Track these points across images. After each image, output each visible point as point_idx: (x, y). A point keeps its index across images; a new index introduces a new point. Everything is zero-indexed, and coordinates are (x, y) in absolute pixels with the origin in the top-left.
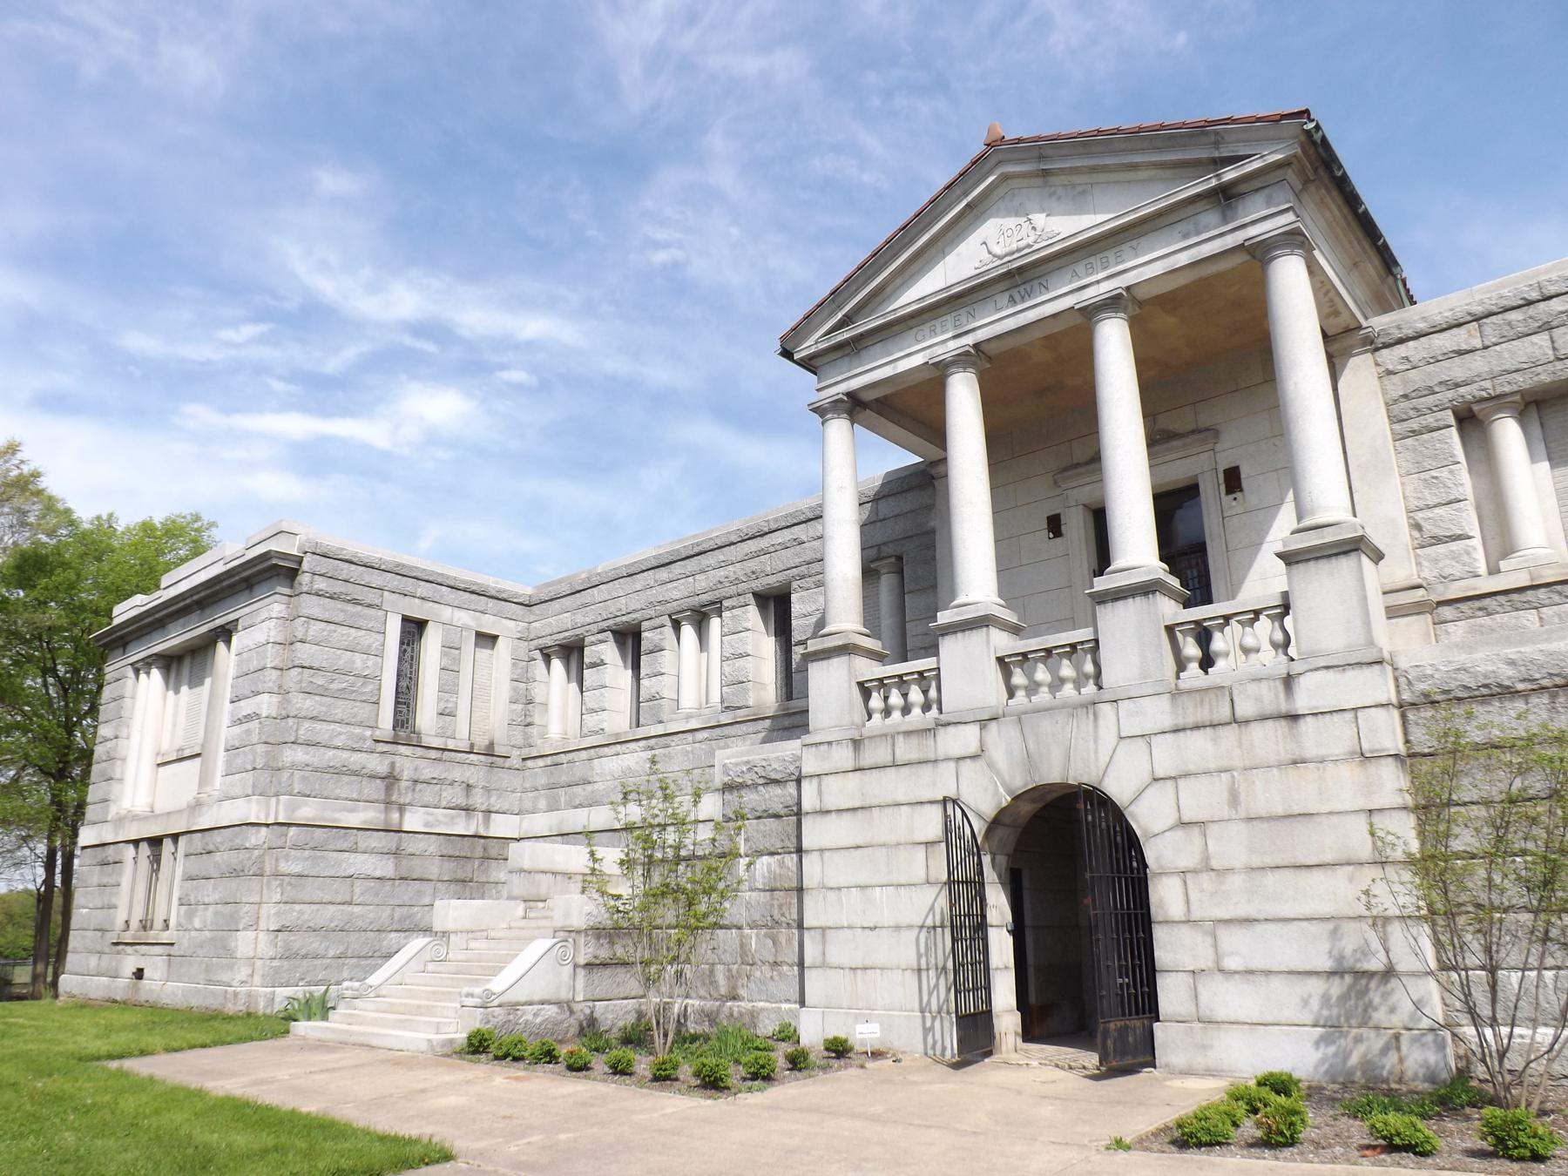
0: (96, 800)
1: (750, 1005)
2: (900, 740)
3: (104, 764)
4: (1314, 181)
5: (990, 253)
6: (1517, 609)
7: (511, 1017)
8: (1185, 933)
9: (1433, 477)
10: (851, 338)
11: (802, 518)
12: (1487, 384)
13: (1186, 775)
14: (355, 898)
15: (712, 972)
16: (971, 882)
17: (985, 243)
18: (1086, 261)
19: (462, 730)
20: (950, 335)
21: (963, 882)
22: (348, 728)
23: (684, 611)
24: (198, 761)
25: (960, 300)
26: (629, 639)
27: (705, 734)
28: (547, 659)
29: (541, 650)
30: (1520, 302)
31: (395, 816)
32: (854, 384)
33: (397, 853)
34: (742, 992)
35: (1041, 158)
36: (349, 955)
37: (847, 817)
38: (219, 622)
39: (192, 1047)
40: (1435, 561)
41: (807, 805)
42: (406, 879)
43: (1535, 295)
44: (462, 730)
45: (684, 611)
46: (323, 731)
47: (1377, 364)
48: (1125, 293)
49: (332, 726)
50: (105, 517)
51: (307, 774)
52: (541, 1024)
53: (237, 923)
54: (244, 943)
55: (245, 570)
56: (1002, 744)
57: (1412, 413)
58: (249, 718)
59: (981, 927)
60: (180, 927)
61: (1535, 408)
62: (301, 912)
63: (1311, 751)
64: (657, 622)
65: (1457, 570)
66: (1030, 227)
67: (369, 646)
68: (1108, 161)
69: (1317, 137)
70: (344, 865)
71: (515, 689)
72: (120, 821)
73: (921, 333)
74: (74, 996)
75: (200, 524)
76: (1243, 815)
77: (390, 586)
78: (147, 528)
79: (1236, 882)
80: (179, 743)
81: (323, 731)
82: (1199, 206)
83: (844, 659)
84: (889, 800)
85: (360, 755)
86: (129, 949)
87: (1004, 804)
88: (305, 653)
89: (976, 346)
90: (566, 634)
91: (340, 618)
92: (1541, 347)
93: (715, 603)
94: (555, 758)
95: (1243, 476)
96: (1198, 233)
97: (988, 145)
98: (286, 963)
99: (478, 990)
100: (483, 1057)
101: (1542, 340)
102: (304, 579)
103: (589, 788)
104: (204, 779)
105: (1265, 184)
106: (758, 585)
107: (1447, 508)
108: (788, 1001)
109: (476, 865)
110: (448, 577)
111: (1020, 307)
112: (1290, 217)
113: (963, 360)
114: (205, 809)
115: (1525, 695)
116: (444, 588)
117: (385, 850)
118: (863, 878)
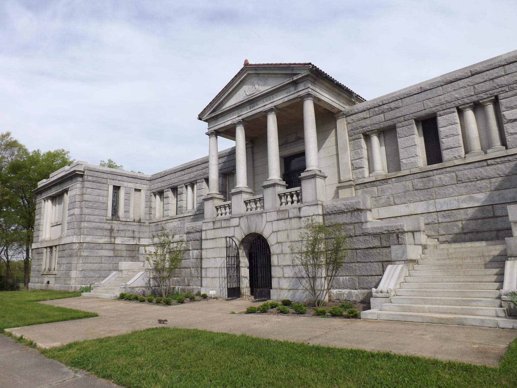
0: (36, 236)
1: (192, 287)
2: (223, 221)
3: (37, 226)
6: (373, 187)
7: (132, 290)
8: (277, 268)
12: (370, 127)
13: (279, 231)
14: (103, 261)
15: (184, 279)
20: (236, 116)
21: (233, 257)
22: (99, 217)
24: (61, 225)
26: (174, 189)
28: (155, 195)
29: (153, 193)
30: (378, 105)
31: (113, 240)
32: (216, 128)
33: (114, 250)
34: (191, 284)
36: (101, 276)
37: (211, 240)
38: (64, 188)
39: (56, 299)
40: (356, 174)
41: (203, 238)
43: (381, 104)
46: (92, 218)
47: (346, 121)
49: (94, 216)
50: (37, 151)
52: (140, 292)
53: (71, 268)
54: (74, 274)
55: (70, 175)
56: (244, 222)
57: (353, 134)
58: (72, 215)
59: (238, 267)
60: (58, 270)
61: (383, 133)
64: (181, 186)
65: (360, 176)
67: (104, 194)
68: (270, 72)
71: (146, 204)
72: (42, 242)
73: (230, 115)
74: (32, 289)
75: (64, 152)
76: (289, 241)
77: (109, 178)
78: (49, 154)
80: (57, 221)
81: (92, 218)
83: (212, 200)
84: (220, 236)
85: (102, 224)
86: (45, 276)
87: (243, 238)
88: (86, 197)
89: (242, 119)
90: (159, 189)
91: (95, 187)
92: (381, 118)
93: (195, 181)
94: (157, 223)
99: (124, 284)
100: (123, 299)
101: (382, 116)
102: (85, 177)
104: (62, 230)
107: (359, 160)
109: (136, 252)
110: (126, 174)
111: (252, 109)
113: (239, 123)
114: (62, 239)
115: (346, 213)
117: (110, 249)
118: (214, 256)
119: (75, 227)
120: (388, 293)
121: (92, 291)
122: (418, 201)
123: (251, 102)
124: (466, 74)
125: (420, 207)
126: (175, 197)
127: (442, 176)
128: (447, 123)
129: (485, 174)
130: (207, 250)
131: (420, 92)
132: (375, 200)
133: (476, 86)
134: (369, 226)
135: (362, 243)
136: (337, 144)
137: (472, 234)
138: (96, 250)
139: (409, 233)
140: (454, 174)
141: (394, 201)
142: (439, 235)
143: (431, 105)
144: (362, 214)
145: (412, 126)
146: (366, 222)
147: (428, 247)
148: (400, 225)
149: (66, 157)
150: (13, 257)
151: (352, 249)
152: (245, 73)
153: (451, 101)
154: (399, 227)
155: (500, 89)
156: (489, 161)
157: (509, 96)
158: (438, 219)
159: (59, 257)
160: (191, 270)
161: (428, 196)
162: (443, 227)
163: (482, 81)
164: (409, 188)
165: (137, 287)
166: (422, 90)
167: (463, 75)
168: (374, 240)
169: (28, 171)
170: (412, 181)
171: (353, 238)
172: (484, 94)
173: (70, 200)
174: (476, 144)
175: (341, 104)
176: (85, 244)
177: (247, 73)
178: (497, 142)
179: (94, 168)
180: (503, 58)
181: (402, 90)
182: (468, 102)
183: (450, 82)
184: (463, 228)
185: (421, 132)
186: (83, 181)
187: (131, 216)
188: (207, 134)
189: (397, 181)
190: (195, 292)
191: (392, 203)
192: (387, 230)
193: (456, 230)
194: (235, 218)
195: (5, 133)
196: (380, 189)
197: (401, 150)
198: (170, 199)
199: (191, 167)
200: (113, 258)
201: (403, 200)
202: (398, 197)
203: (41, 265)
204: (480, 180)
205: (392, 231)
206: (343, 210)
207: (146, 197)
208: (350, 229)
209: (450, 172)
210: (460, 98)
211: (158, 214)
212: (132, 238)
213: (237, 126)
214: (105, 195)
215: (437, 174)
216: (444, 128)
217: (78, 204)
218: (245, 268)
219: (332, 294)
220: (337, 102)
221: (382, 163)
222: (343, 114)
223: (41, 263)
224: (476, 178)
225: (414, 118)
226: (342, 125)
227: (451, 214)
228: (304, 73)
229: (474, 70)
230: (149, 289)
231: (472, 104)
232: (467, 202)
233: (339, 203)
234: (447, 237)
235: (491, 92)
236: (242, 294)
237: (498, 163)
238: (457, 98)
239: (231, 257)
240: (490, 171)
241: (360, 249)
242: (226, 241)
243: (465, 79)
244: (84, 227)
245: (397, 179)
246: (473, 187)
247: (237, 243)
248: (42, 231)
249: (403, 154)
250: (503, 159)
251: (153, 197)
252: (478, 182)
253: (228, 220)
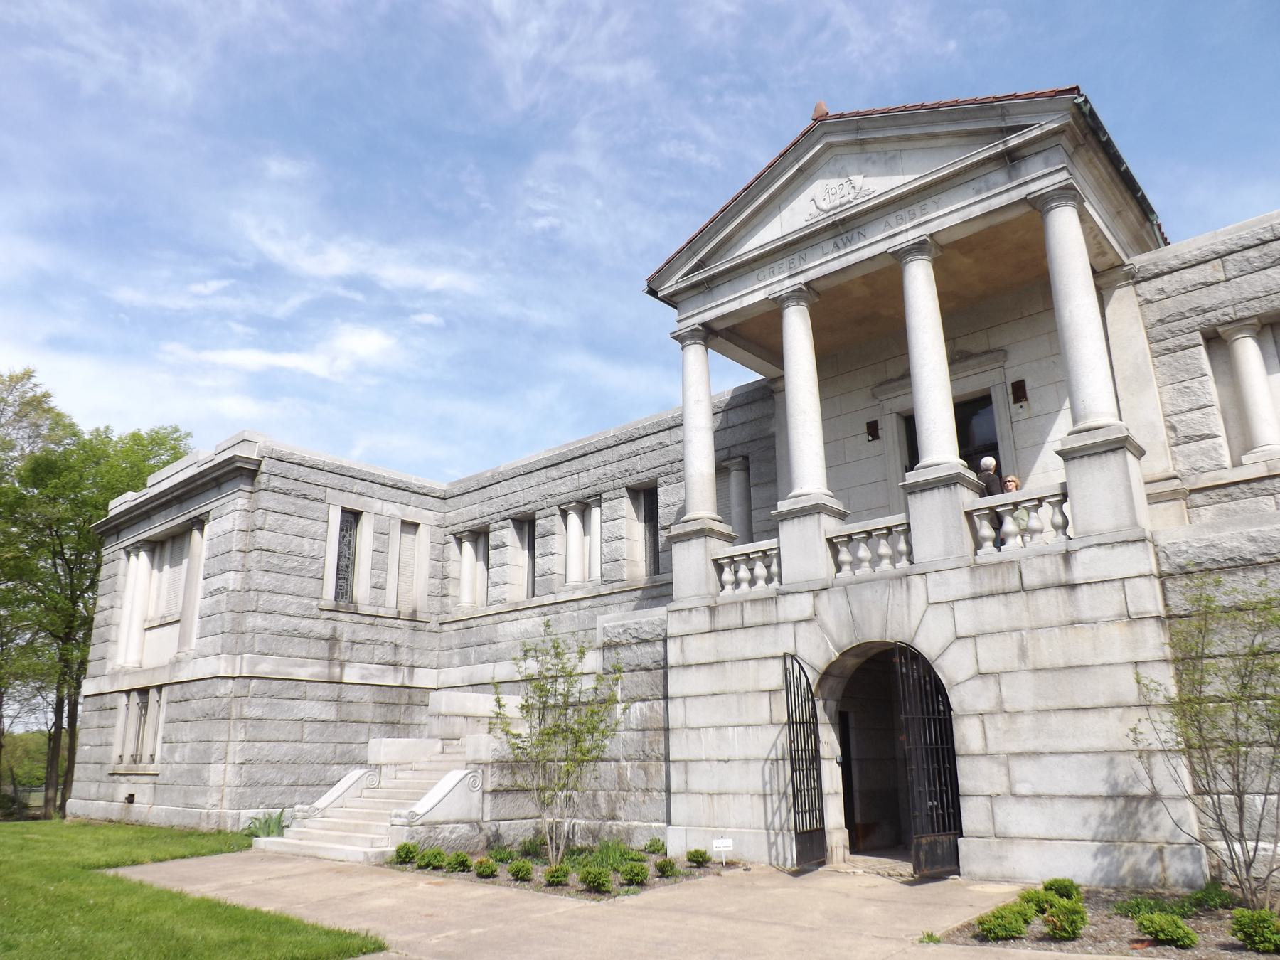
0: (96, 658)
1: (627, 823)
2: (748, 606)
3: (102, 629)
4: (1084, 144)
5: (818, 208)
6: (1257, 496)
8: (983, 764)
10: (704, 279)
11: (666, 426)
12: (1230, 310)
13: (983, 634)
14: (304, 737)
15: (595, 797)
17: (813, 200)
18: (896, 214)
19: (391, 600)
20: (786, 275)
21: (800, 723)
22: (299, 599)
24: (177, 626)
25: (793, 247)
26: (526, 525)
27: (588, 603)
28: (459, 542)
29: (454, 535)
30: (1256, 242)
31: (337, 670)
33: (338, 701)
34: (620, 813)
35: (859, 130)
36: (300, 783)
37: (705, 670)
38: (194, 514)
39: (174, 858)
40: (1188, 456)
41: (672, 660)
43: (1269, 236)
44: (391, 600)
46: (278, 601)
47: (1138, 295)
48: (928, 239)
49: (286, 598)
50: (102, 429)
51: (265, 636)
52: (456, 840)
54: (216, 773)
57: (1167, 335)
60: (163, 761)
63: (1086, 613)
64: (548, 511)
66: (851, 186)
67: (315, 533)
68: (914, 131)
69: (1086, 109)
71: (433, 567)
72: (115, 675)
74: (78, 817)
75: (178, 434)
76: (1030, 667)
77: (331, 484)
79: (1026, 722)
81: (278, 601)
82: (990, 167)
83: (702, 540)
84: (739, 656)
86: (123, 779)
87: (834, 659)
88: (263, 538)
89: (807, 284)
90: (475, 522)
91: (292, 509)
94: (466, 623)
95: (1028, 388)
96: (989, 189)
97: (815, 120)
99: (405, 812)
100: (409, 866)
102: (262, 478)
103: (494, 647)
104: (183, 640)
105: (1042, 149)
106: (630, 481)
107: (1197, 412)
108: (657, 820)
110: (379, 476)
112: (1064, 175)
114: (183, 665)
117: (329, 698)
118: (718, 720)
119: (227, 628)
126: (521, 540)
130: (688, 700)
138: (289, 701)
150: (17, 720)
152: (817, 142)
160: (619, 768)
165: (447, 823)
169: (78, 479)
173: (210, 548)
176: (255, 681)
187: (390, 603)
190: (640, 842)
194: (798, 596)
200: (335, 726)
203: (109, 744)
206: (1249, 556)
207: (432, 547)
212: (392, 667)
218: (830, 762)
223: (110, 739)
239: (796, 723)
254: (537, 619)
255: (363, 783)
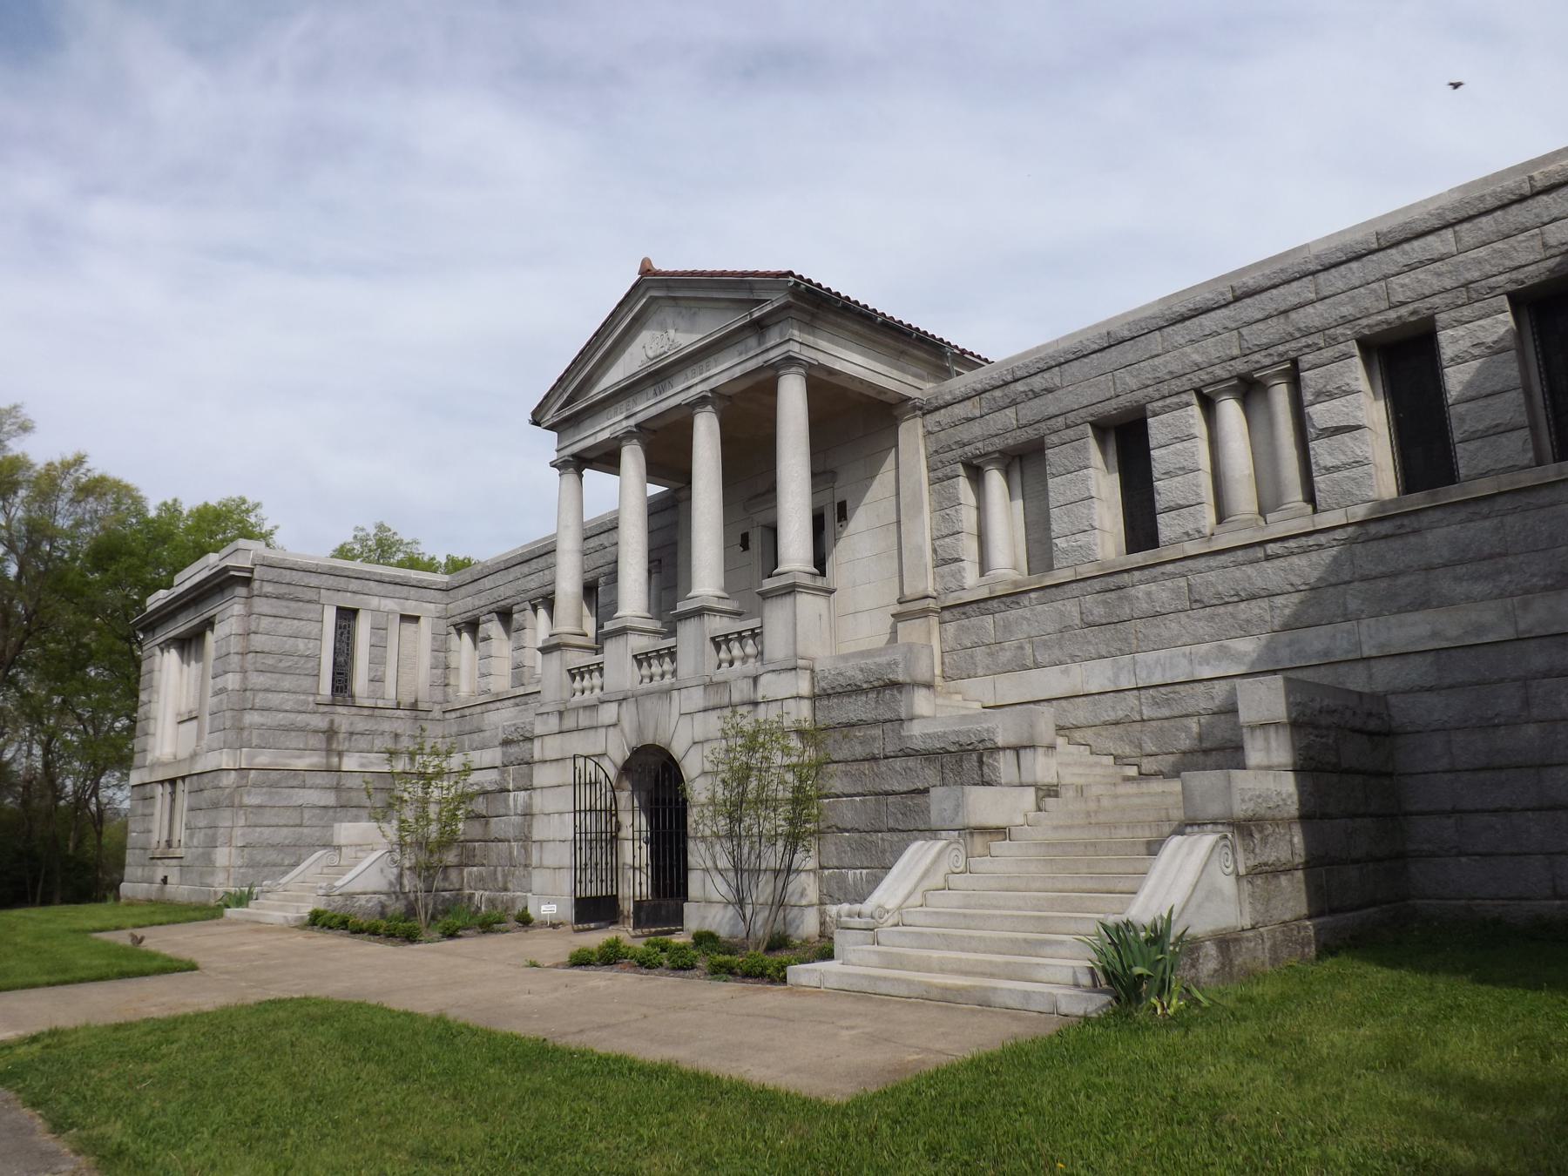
2: (581, 711)
6: (983, 615)
9: (1347, 407)
11: (605, 528)
12: (980, 445)
15: (495, 871)
16: (590, 810)
19: (390, 692)
21: (601, 811)
23: (538, 598)
24: (195, 723)
26: (505, 616)
29: (454, 626)
31: (335, 760)
32: (576, 448)
33: (337, 788)
34: (510, 886)
37: (554, 764)
38: (206, 616)
39: (152, 925)
40: (942, 577)
42: (345, 807)
43: (1009, 378)
44: (390, 692)
45: (538, 598)
46: (275, 699)
49: (281, 695)
51: (261, 731)
52: (372, 907)
53: (215, 841)
54: (222, 856)
57: (939, 465)
58: (223, 690)
59: (614, 839)
62: (261, 833)
67: (310, 633)
68: (701, 294)
70: (295, 798)
71: (435, 658)
72: (153, 766)
80: (183, 709)
81: (275, 699)
85: (304, 715)
86: (159, 862)
88: (258, 641)
89: (637, 426)
90: (469, 614)
91: (285, 612)
94: (462, 712)
98: (251, 870)
101: (1010, 412)
102: (256, 585)
103: (481, 734)
107: (952, 538)
113: (629, 435)
114: (198, 758)
116: (372, 583)
119: (228, 724)
120: (872, 917)
121: (252, 903)
122: (1094, 656)
123: (657, 376)
124: (1221, 297)
125: (1095, 676)
127: (1153, 587)
128: (1170, 436)
129: (1260, 583)
131: (1106, 345)
132: (988, 654)
133: (1244, 331)
134: (916, 729)
135: (899, 777)
136: (898, 494)
137: (1222, 754)
138: (287, 790)
139: (1008, 751)
140: (1182, 582)
141: (1034, 656)
142: (1143, 756)
143: (1133, 383)
144: (903, 698)
145: (1084, 443)
146: (911, 719)
147: (1062, 791)
148: (988, 730)
149: (253, 520)
151: (876, 794)
153: (1182, 373)
154: (985, 736)
155: (1304, 341)
156: (1271, 545)
157: (1324, 361)
158: (1141, 710)
159: (191, 809)
161: (1119, 645)
162: (1152, 732)
163: (1260, 316)
164: (1073, 620)
165: (365, 893)
166: (1111, 341)
167: (1213, 299)
168: (926, 770)
170: (1080, 600)
171: (882, 762)
172: (1263, 353)
174: (1243, 498)
175: (910, 379)
176: (253, 771)
177: (648, 296)
178: (1295, 494)
179: (281, 560)
180: (1314, 251)
181: (1064, 339)
182: (1225, 377)
183: (1180, 318)
184: (1201, 738)
185: (1113, 460)
186: (249, 597)
188: (553, 465)
189: (1043, 601)
191: (1029, 662)
192: (958, 742)
193: (1185, 743)
195: (70, 457)
196: (1002, 623)
197: (1054, 513)
198: (494, 643)
199: (546, 554)
200: (335, 812)
201: (1057, 653)
202: (1045, 643)
203: (150, 831)
204: (1247, 600)
205: (968, 745)
207: (434, 638)
208: (874, 739)
209: (1172, 576)
210: (1204, 365)
211: (465, 687)
213: (624, 443)
214: (314, 632)
215: (1141, 582)
216: (1163, 451)
217: (235, 659)
219: (828, 919)
220: (895, 374)
221: (1014, 546)
222: (915, 408)
224: (1237, 595)
225: (1090, 419)
226: (912, 438)
227: (1172, 695)
228: (777, 299)
229: (1241, 284)
230: (397, 897)
231: (1235, 382)
232: (1212, 662)
233: (850, 664)
234: (1162, 760)
235: (1281, 348)
236: (626, 913)
237: (1292, 554)
238: (1196, 364)
240: (1269, 575)
241: (894, 793)
242: (575, 768)
243: (1218, 311)
244: (251, 725)
245: (1042, 593)
246: (1230, 620)
247: (612, 773)
248: (154, 735)
249: (1059, 523)
250: (1303, 541)
251: (454, 636)
252: (1243, 605)
253: (592, 707)
254: (512, 709)
255: (324, 862)
